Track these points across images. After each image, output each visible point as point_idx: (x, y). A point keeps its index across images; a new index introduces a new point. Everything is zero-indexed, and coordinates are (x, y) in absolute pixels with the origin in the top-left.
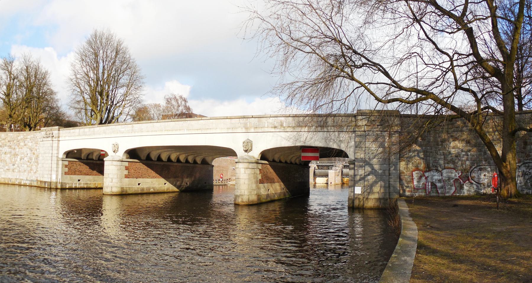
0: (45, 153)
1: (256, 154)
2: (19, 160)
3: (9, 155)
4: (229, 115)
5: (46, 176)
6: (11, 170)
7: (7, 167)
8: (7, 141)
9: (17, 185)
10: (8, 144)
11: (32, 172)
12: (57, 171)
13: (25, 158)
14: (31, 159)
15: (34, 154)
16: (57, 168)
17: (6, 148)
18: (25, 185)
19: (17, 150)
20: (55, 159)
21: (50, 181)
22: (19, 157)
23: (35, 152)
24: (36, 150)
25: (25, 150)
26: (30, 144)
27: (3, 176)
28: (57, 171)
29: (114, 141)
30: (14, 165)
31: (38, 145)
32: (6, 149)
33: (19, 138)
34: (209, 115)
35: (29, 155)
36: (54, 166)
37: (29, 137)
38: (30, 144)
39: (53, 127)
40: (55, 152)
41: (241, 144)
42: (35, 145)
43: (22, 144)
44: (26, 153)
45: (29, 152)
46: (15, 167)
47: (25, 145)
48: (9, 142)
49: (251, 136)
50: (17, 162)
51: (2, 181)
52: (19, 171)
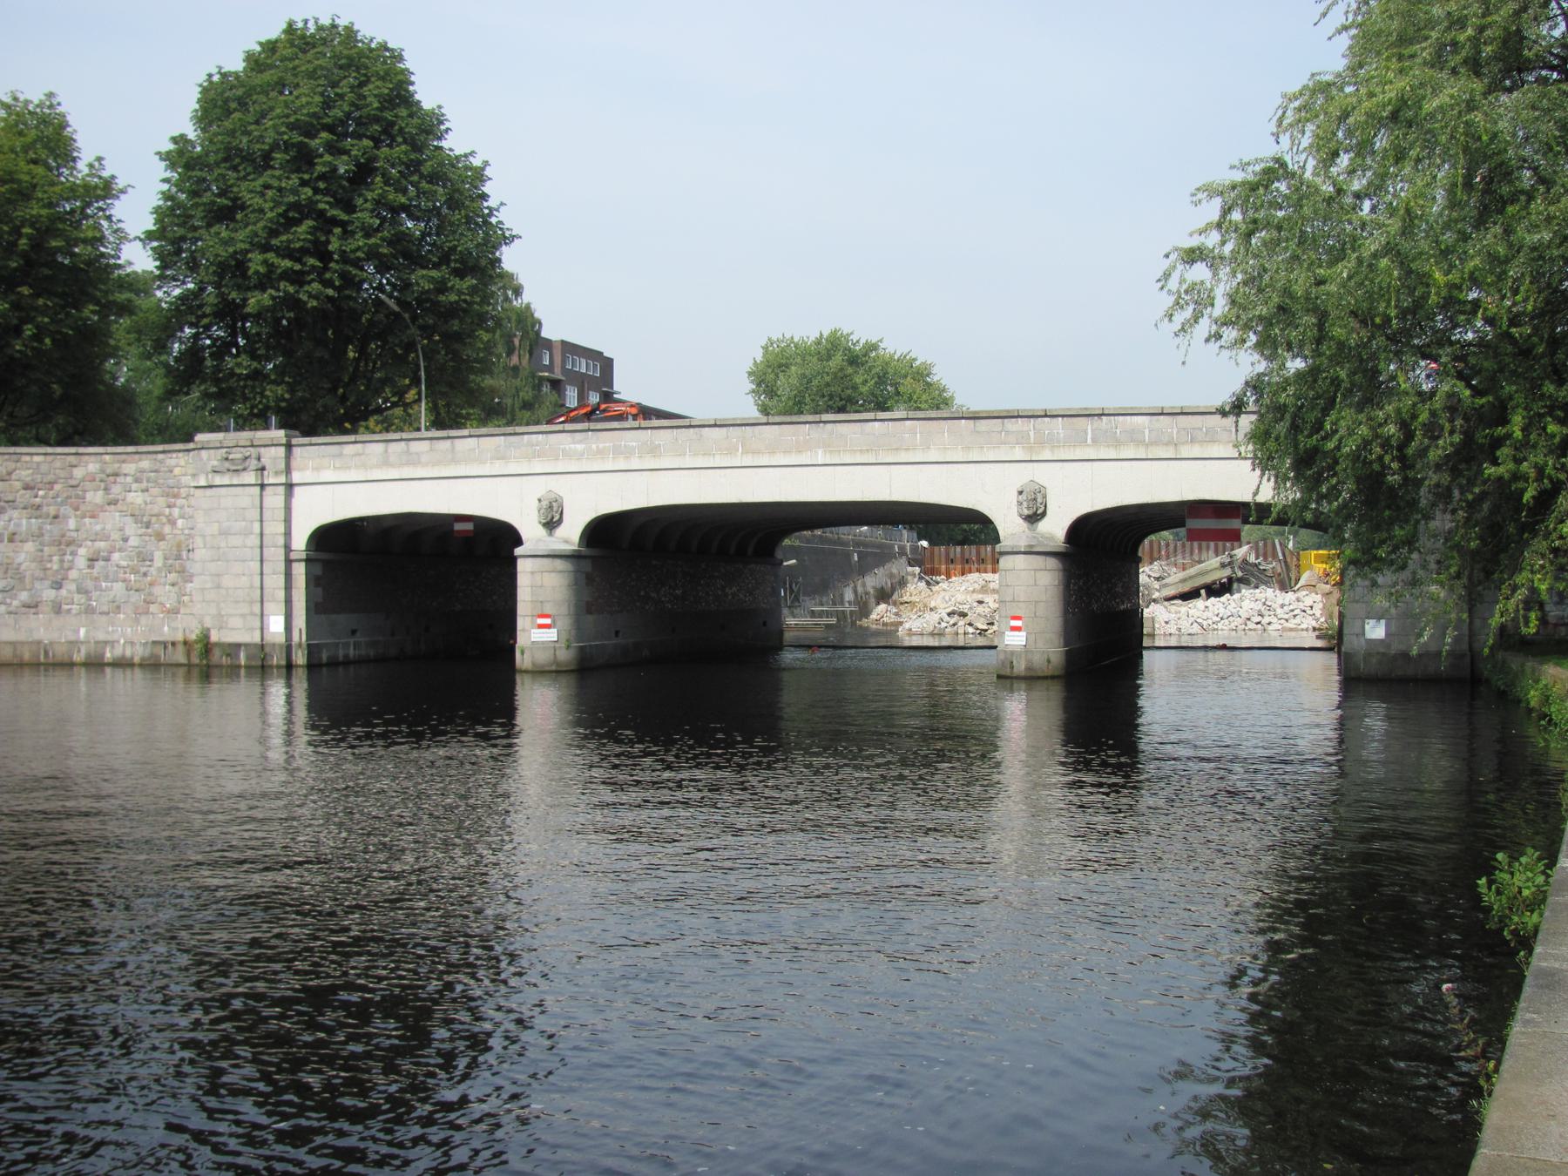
0: (224, 533)
1: (1056, 527)
2: (81, 562)
3: (30, 546)
4: (1095, 404)
5: (236, 622)
6: (45, 608)
7: (24, 596)
8: (18, 485)
9: (1018, 678)
10: (24, 497)
11: (153, 608)
12: (288, 602)
13: (116, 556)
14: (145, 557)
15: (160, 537)
16: (288, 587)
17: (15, 514)
18: (122, 664)
19: (72, 524)
20: (276, 555)
21: (257, 639)
22: (82, 551)
23: (167, 529)
24: (173, 523)
25: (112, 520)
26: (136, 498)
27: (8, 635)
28: (288, 602)
29: (1022, 475)
30: (58, 585)
31: (179, 502)
32: (19, 520)
33: (78, 473)
34: (698, 413)
35: (134, 541)
36: (275, 582)
37: (130, 468)
38: (136, 498)
39: (262, 435)
40: (275, 528)
41: (1014, 497)
42: (162, 501)
43: (95, 497)
44: (115, 536)
45: (131, 529)
46: (64, 592)
47: (114, 502)
48: (27, 487)
49: (1043, 475)
50: (73, 574)
51: (7, 654)
52: (89, 610)
